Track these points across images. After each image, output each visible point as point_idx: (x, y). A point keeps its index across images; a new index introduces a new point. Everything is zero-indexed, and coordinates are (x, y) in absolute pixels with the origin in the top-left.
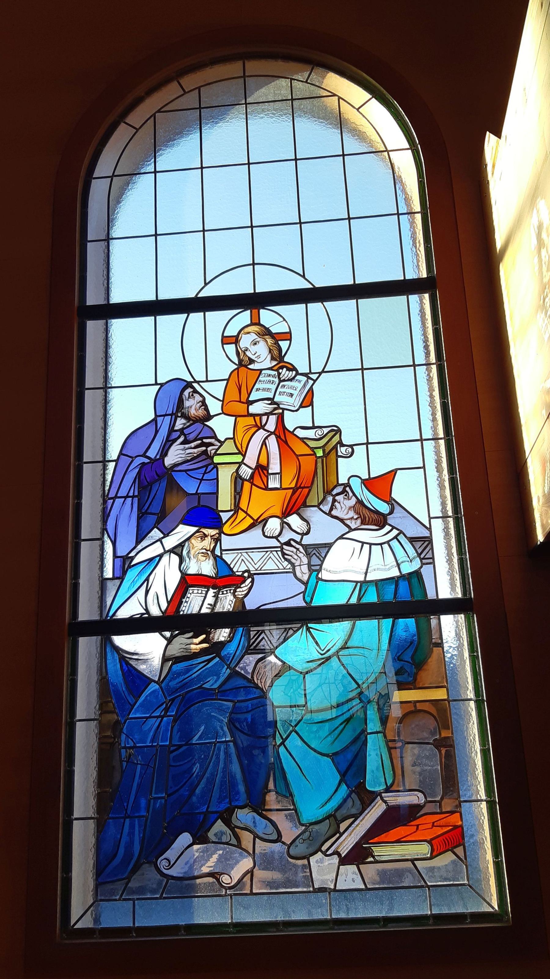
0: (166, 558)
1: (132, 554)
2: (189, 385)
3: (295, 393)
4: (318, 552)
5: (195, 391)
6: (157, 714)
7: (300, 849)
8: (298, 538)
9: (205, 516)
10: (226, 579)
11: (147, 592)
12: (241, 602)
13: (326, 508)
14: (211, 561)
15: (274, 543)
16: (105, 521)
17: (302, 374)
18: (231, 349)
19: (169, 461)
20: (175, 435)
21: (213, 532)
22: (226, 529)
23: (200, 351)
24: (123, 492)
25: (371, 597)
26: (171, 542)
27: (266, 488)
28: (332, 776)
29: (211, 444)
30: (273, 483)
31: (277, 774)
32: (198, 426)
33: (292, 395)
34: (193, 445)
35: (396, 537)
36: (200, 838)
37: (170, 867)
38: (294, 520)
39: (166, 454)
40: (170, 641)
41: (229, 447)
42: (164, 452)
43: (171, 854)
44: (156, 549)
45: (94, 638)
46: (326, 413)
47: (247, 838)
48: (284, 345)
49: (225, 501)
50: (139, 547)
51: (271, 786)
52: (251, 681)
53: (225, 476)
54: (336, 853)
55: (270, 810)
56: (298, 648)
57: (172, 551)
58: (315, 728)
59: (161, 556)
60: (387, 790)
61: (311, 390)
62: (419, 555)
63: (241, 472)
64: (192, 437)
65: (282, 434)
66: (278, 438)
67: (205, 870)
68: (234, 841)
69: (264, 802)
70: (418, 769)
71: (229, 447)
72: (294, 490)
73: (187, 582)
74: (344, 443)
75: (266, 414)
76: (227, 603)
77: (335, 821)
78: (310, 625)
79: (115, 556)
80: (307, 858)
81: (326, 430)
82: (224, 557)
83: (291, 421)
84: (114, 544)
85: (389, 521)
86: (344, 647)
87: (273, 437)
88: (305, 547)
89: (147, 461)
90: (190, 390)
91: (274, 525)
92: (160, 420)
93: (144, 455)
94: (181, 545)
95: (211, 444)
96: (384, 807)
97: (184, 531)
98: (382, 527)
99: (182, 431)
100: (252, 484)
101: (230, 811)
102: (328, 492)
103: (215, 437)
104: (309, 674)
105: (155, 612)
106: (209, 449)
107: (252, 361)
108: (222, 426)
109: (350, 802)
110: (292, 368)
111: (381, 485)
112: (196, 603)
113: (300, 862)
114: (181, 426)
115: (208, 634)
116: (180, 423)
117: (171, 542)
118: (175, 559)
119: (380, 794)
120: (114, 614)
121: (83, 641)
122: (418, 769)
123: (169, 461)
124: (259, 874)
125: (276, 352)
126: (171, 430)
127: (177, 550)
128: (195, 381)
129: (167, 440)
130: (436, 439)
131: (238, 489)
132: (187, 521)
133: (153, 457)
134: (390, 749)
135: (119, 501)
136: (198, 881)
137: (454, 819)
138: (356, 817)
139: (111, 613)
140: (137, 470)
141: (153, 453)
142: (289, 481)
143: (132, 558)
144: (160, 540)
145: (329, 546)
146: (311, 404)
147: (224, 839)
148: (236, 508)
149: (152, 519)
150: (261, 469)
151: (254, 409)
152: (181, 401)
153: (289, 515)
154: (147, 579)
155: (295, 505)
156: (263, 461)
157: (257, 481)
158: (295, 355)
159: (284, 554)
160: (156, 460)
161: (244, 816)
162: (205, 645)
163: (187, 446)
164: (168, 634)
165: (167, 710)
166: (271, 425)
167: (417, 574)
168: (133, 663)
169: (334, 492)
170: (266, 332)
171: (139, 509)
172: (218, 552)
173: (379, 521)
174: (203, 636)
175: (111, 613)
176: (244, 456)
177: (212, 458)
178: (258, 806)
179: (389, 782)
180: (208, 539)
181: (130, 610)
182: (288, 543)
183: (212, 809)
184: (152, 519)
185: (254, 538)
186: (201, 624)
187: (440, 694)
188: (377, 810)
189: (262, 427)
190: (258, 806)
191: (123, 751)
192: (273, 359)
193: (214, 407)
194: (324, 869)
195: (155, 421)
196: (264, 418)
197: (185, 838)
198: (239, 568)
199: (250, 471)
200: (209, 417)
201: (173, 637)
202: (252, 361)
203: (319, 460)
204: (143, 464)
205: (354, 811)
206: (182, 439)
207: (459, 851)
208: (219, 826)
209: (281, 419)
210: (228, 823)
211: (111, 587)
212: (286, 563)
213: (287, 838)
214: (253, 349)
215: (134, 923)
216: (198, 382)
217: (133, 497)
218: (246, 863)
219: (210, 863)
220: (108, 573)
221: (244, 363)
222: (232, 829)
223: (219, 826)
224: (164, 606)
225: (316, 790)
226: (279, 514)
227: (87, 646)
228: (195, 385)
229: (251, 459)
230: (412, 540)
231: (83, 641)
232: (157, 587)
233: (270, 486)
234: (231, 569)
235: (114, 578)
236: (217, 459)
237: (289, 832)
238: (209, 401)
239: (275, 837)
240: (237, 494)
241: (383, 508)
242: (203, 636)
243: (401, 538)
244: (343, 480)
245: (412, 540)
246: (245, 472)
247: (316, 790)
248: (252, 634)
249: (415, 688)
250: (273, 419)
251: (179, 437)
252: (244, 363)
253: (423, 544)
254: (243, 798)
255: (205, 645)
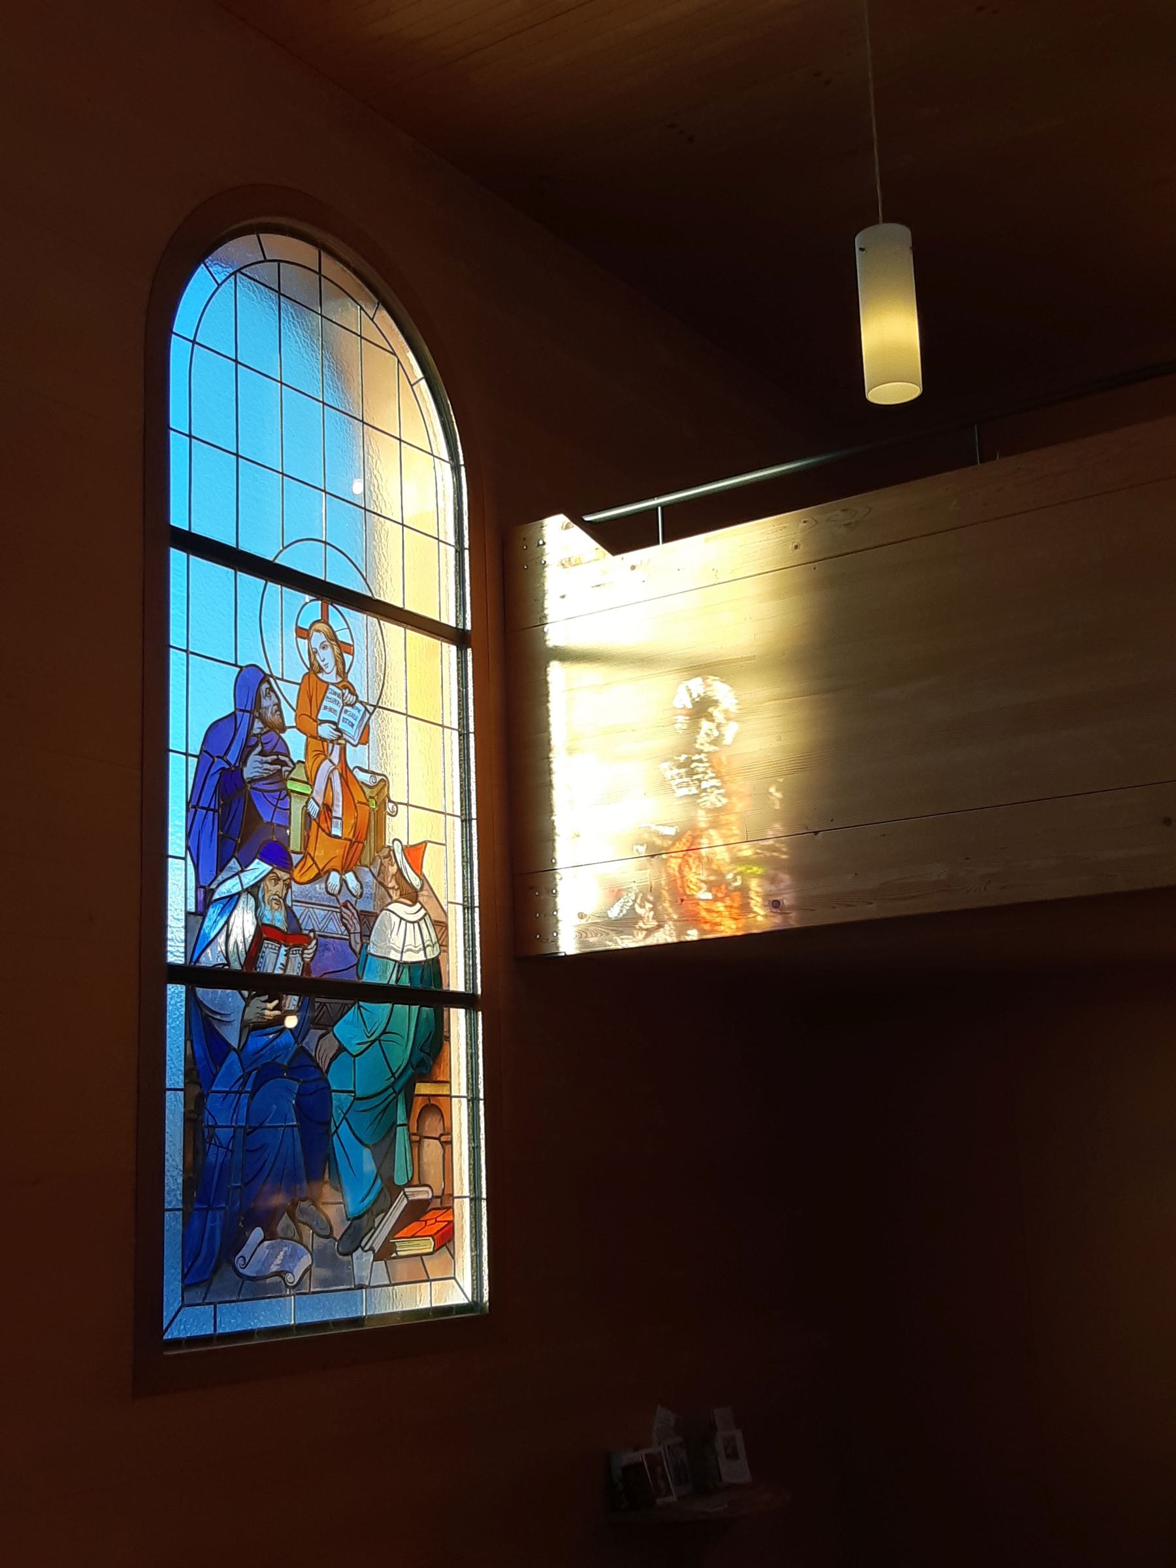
1: (213, 886)
3: (356, 723)
6: (235, 1089)
17: (361, 703)
18: (303, 643)
26: (249, 878)
33: (352, 725)
34: (269, 759)
35: (423, 918)
36: (270, 1235)
39: (245, 764)
41: (299, 773)
42: (243, 759)
43: (245, 1251)
48: (348, 658)
49: (295, 844)
50: (220, 878)
55: (327, 1204)
61: (367, 725)
64: (268, 748)
67: (274, 1268)
68: (297, 1237)
73: (264, 932)
74: (392, 799)
75: (332, 741)
78: (361, 1003)
80: (350, 1254)
82: (294, 908)
85: (420, 899)
86: (384, 1032)
91: (334, 878)
94: (256, 885)
97: (259, 868)
98: (414, 903)
103: (288, 755)
106: (284, 769)
107: (321, 670)
108: (295, 743)
112: (275, 961)
113: (346, 1258)
114: (258, 731)
120: (198, 960)
124: (316, 1271)
127: (253, 890)
128: (272, 676)
132: (265, 858)
136: (268, 1281)
143: (213, 891)
144: (237, 874)
147: (290, 1235)
148: (305, 853)
153: (347, 872)
154: (227, 922)
163: (265, 759)
164: (246, 993)
165: (244, 1084)
167: (436, 962)
170: (332, 637)
174: (276, 1002)
176: (312, 786)
186: (275, 987)
188: (400, 1205)
191: (206, 1130)
192: (338, 673)
193: (289, 718)
197: (257, 1233)
201: (251, 997)
206: (259, 749)
208: (285, 1220)
209: (343, 751)
210: (292, 1217)
212: (343, 928)
214: (321, 652)
215: (215, 1330)
216: (276, 679)
218: (307, 1260)
219: (278, 1261)
221: (315, 669)
223: (285, 1220)
228: (272, 680)
232: (237, 935)
233: (334, 833)
234: (300, 926)
239: (328, 1233)
242: (276, 1002)
246: (314, 809)
252: (315, 669)
255: (277, 1012)
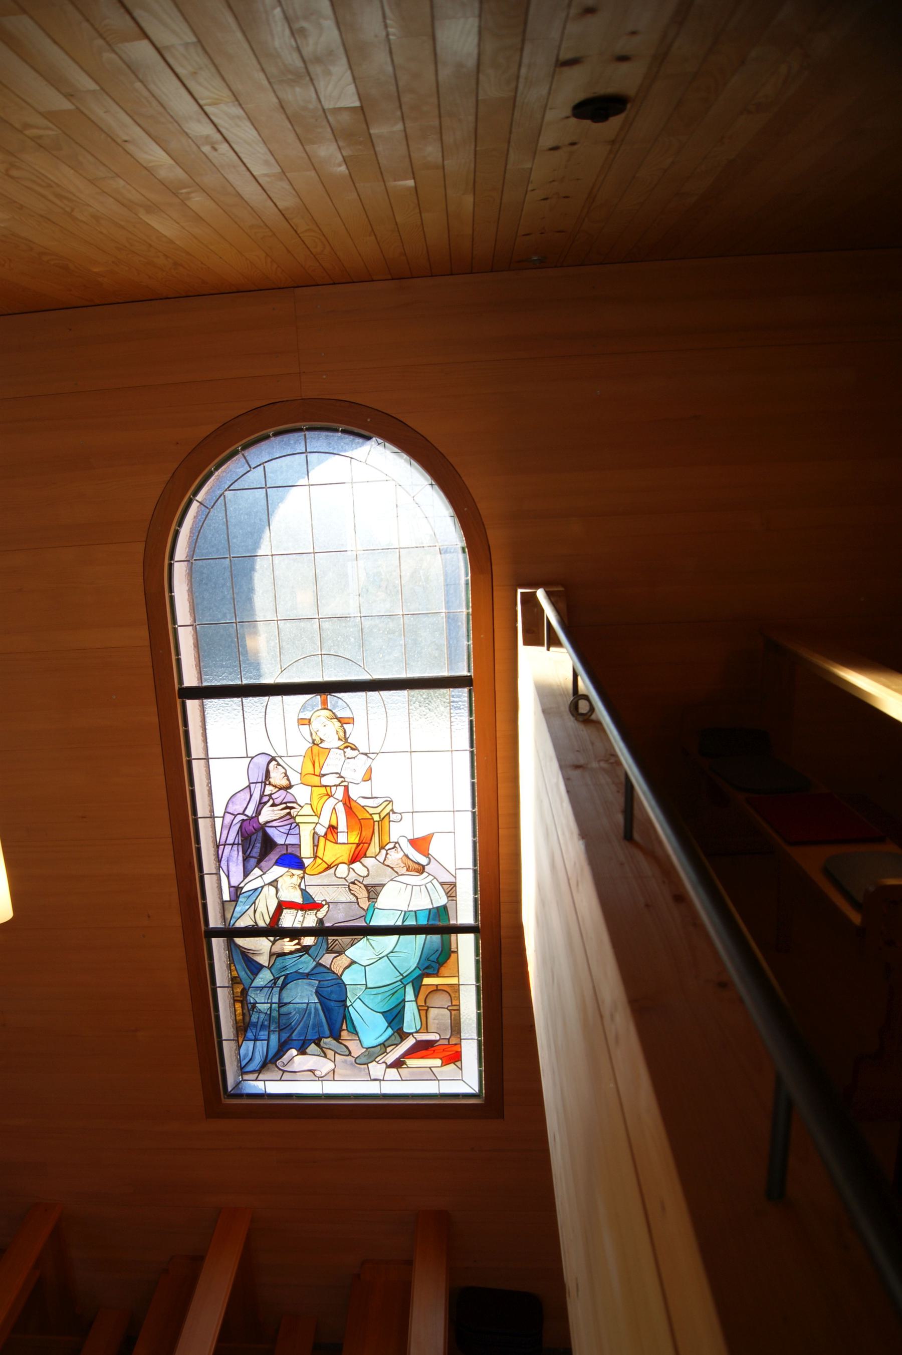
0: (266, 888)
2: (273, 759)
4: (373, 891)
5: (279, 764)
7: (363, 1060)
8: (361, 879)
9: (292, 861)
10: (309, 905)
11: (255, 911)
12: (321, 921)
13: (381, 858)
14: (299, 892)
15: (343, 882)
16: (219, 861)
18: (305, 729)
19: (262, 819)
20: (265, 799)
21: (300, 872)
22: (307, 871)
23: (279, 726)
24: (230, 841)
25: (411, 922)
26: (269, 877)
27: (336, 843)
28: (382, 1023)
29: (293, 808)
30: (342, 838)
31: (348, 1022)
32: (282, 793)
37: (285, 1065)
38: (357, 866)
40: (273, 943)
42: (258, 812)
44: (258, 883)
45: (221, 939)
46: (381, 787)
47: (330, 1054)
49: (306, 851)
50: (246, 880)
51: (344, 1027)
52: (330, 969)
53: (306, 833)
54: (384, 1062)
56: (362, 950)
57: (270, 884)
58: (372, 997)
59: (262, 887)
60: (417, 1032)
62: (447, 894)
63: (317, 830)
65: (348, 802)
66: (345, 804)
68: (322, 1054)
69: (340, 1036)
70: (436, 1021)
71: (307, 810)
72: (358, 845)
73: (282, 906)
75: (336, 786)
76: (310, 920)
77: (384, 1047)
79: (230, 886)
80: (367, 1064)
81: (382, 800)
83: (354, 793)
84: (228, 877)
86: (392, 952)
87: (341, 803)
88: (366, 886)
89: (245, 818)
90: (274, 763)
91: (342, 870)
92: (252, 786)
93: (243, 814)
95: (293, 808)
96: (414, 1041)
99: (270, 795)
100: (326, 839)
101: (320, 1039)
102: (382, 848)
104: (369, 967)
105: (261, 924)
106: (292, 811)
107: (322, 741)
108: (301, 793)
109: (393, 1038)
110: (354, 748)
111: (421, 844)
112: (289, 920)
115: (300, 940)
116: (269, 790)
117: (269, 877)
118: (273, 890)
119: (412, 1034)
121: (215, 941)
122: (436, 1021)
123: (262, 819)
125: (342, 734)
126: (262, 796)
127: (274, 883)
129: (260, 803)
130: (238, 844)
131: (316, 843)
132: (279, 863)
133: (250, 815)
134: (419, 1010)
135: (228, 848)
137: (456, 1048)
138: (397, 1045)
139: (232, 922)
140: (239, 825)
141: (250, 812)
142: (354, 838)
143: (242, 888)
145: (383, 885)
146: (370, 779)
148: (315, 857)
149: (253, 861)
150: (333, 829)
151: (325, 781)
152: (268, 772)
154: (254, 903)
155: (356, 858)
156: (334, 823)
157: (330, 836)
158: (356, 735)
159: (350, 890)
160: (252, 817)
161: (328, 1042)
162: (299, 947)
164: (272, 939)
166: (339, 793)
167: (445, 907)
168: (250, 955)
169: (387, 848)
171: (244, 853)
172: (303, 886)
173: (421, 869)
175: (232, 922)
177: (294, 818)
178: (337, 1038)
179: (418, 1028)
180: (295, 877)
181: (244, 922)
182: (353, 883)
183: (309, 1037)
184: (253, 861)
185: (327, 877)
186: (295, 933)
187: (454, 981)
188: (409, 1042)
189: (330, 796)
190: (337, 1038)
192: (339, 739)
193: (295, 778)
194: (377, 1069)
195: (249, 786)
196: (334, 789)
198: (318, 899)
199: (325, 830)
200: (290, 787)
202: (322, 741)
203: (376, 824)
204: (243, 820)
205: (396, 1042)
206: (271, 802)
207: (458, 1063)
210: (318, 1045)
211: (229, 907)
212: (352, 896)
213: (355, 1054)
216: (280, 757)
217: (238, 844)
220: (226, 897)
222: (321, 1048)
224: (268, 921)
225: (371, 1027)
226: (346, 861)
227: (218, 944)
228: (278, 759)
229: (325, 821)
230: (442, 884)
231: (215, 941)
235: (230, 901)
236: (298, 819)
237: (357, 1051)
238: (290, 773)
240: (316, 846)
241: (423, 860)
243: (435, 882)
244: (393, 839)
245: (442, 884)
246: (321, 831)
247: (371, 1027)
248: (330, 941)
249: (438, 977)
250: (341, 790)
251: (268, 801)
253: (451, 889)
254: (327, 1033)
255: (299, 947)
